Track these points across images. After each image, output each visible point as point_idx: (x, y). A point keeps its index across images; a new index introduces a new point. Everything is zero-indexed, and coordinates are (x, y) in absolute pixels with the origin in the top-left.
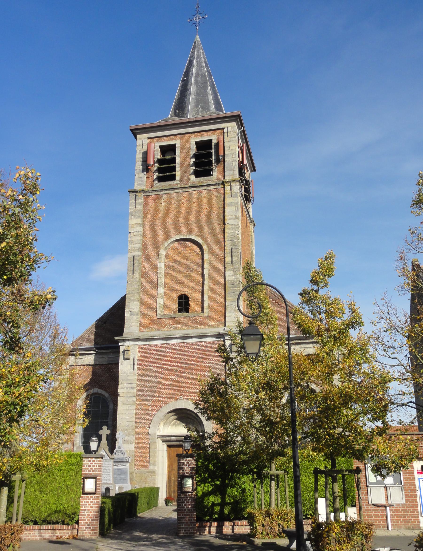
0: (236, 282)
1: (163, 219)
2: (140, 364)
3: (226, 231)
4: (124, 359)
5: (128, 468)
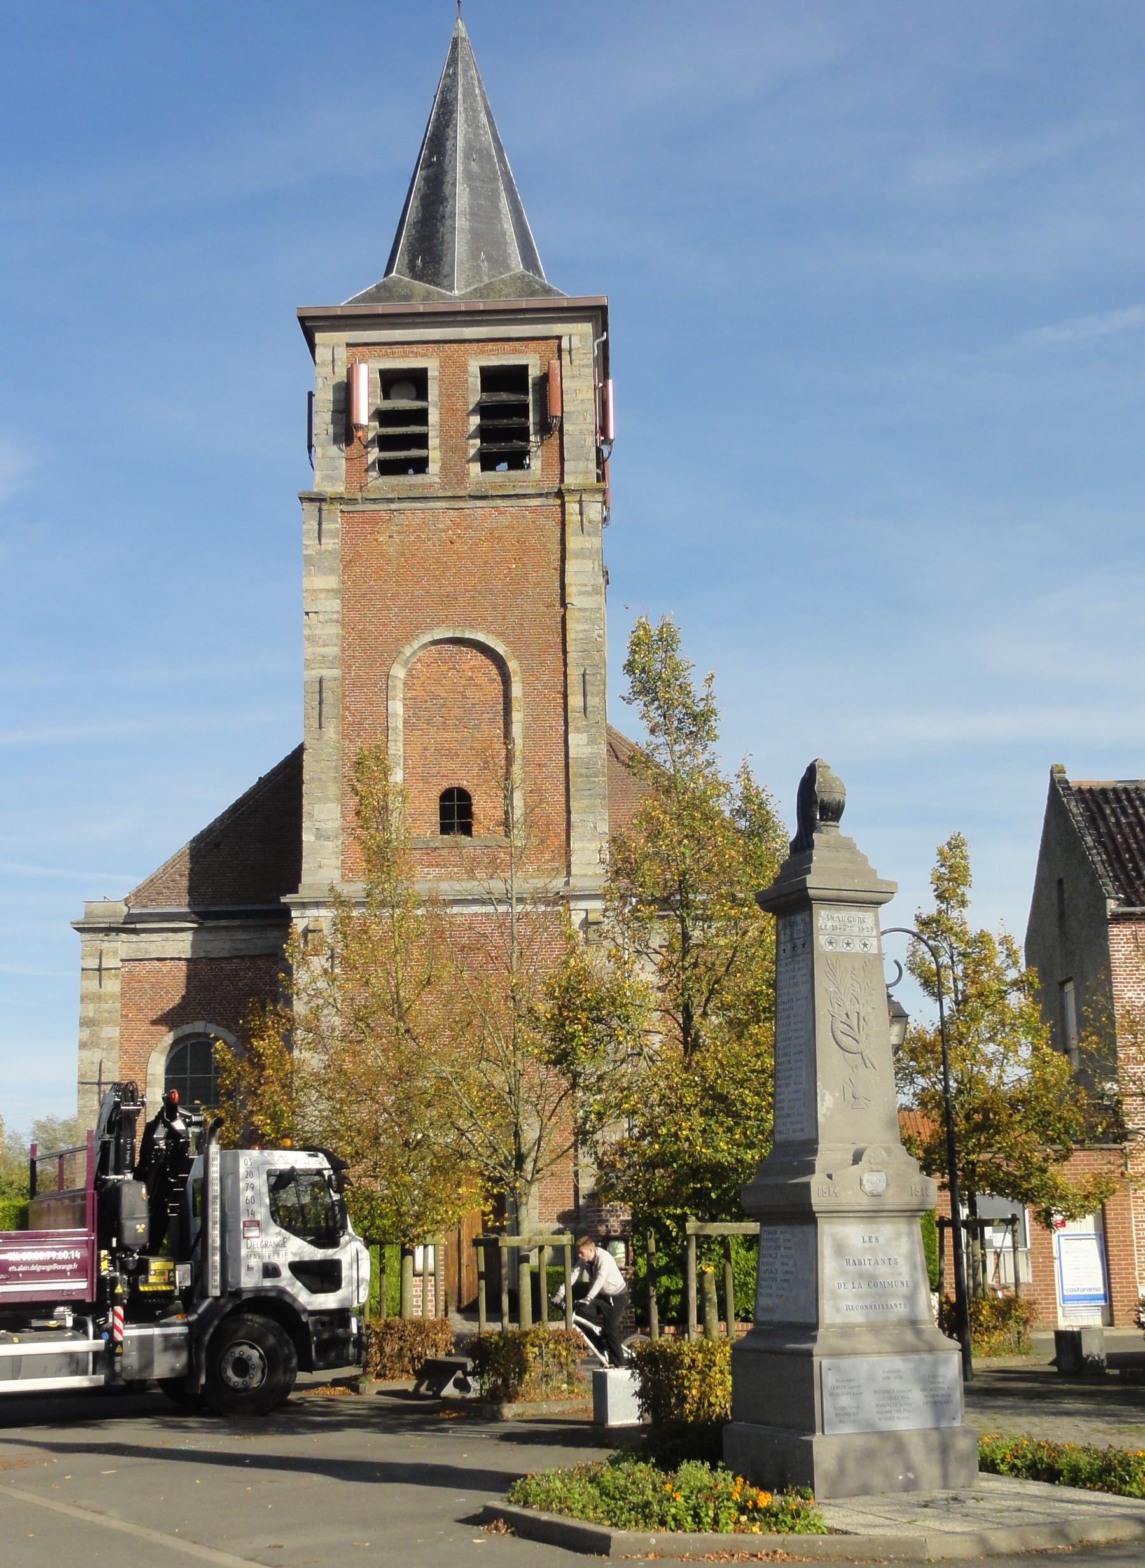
0: (596, 763)
1: (397, 581)
3: (570, 625)
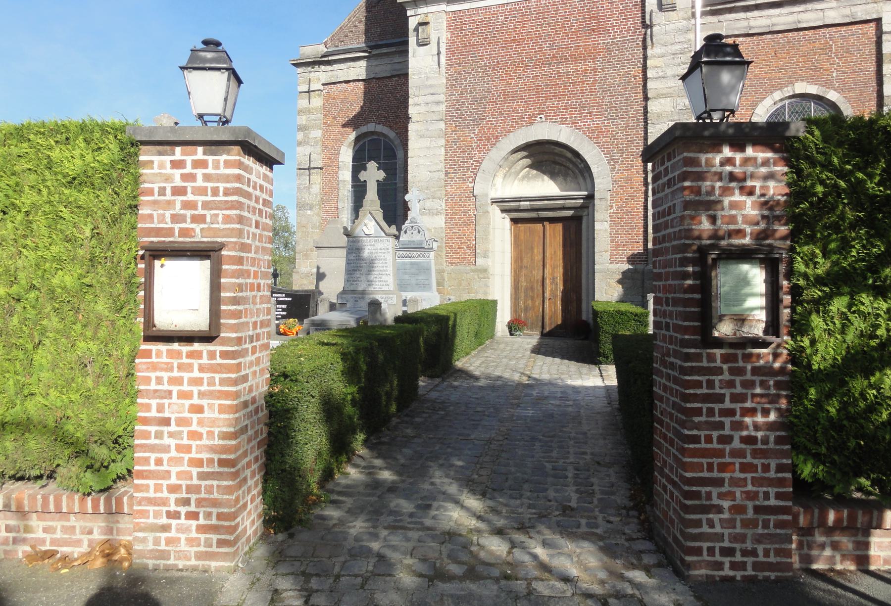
2: (451, 52)
4: (419, 45)
5: (433, 262)
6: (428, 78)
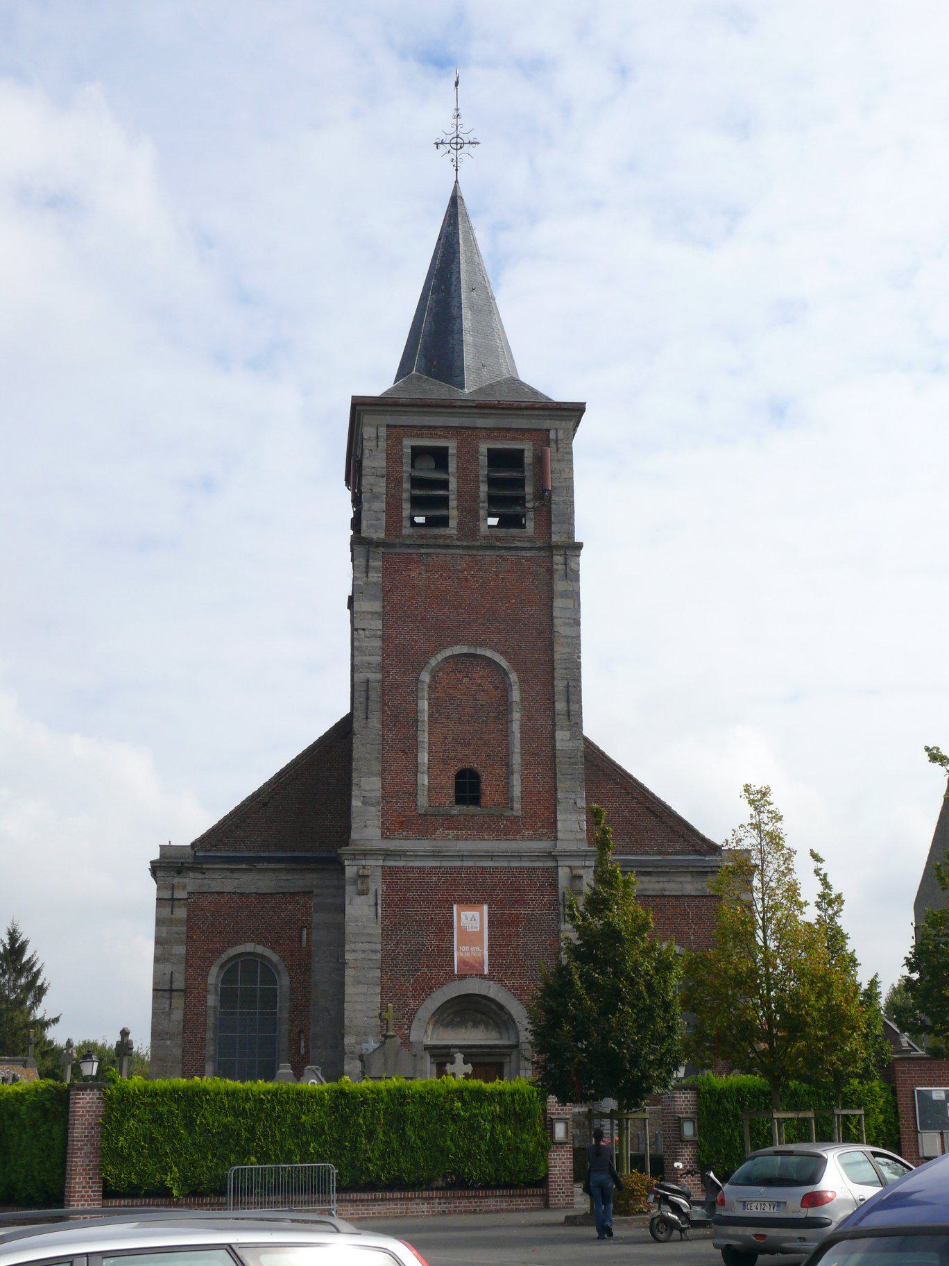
6: (365, 927)
